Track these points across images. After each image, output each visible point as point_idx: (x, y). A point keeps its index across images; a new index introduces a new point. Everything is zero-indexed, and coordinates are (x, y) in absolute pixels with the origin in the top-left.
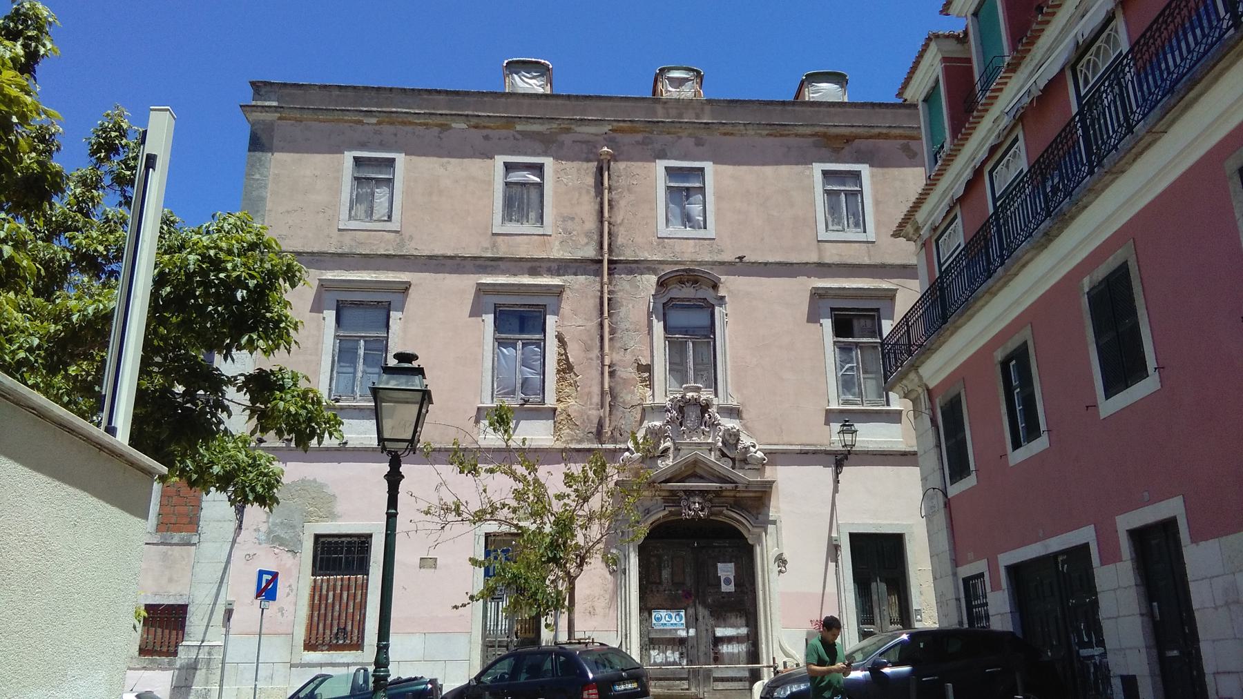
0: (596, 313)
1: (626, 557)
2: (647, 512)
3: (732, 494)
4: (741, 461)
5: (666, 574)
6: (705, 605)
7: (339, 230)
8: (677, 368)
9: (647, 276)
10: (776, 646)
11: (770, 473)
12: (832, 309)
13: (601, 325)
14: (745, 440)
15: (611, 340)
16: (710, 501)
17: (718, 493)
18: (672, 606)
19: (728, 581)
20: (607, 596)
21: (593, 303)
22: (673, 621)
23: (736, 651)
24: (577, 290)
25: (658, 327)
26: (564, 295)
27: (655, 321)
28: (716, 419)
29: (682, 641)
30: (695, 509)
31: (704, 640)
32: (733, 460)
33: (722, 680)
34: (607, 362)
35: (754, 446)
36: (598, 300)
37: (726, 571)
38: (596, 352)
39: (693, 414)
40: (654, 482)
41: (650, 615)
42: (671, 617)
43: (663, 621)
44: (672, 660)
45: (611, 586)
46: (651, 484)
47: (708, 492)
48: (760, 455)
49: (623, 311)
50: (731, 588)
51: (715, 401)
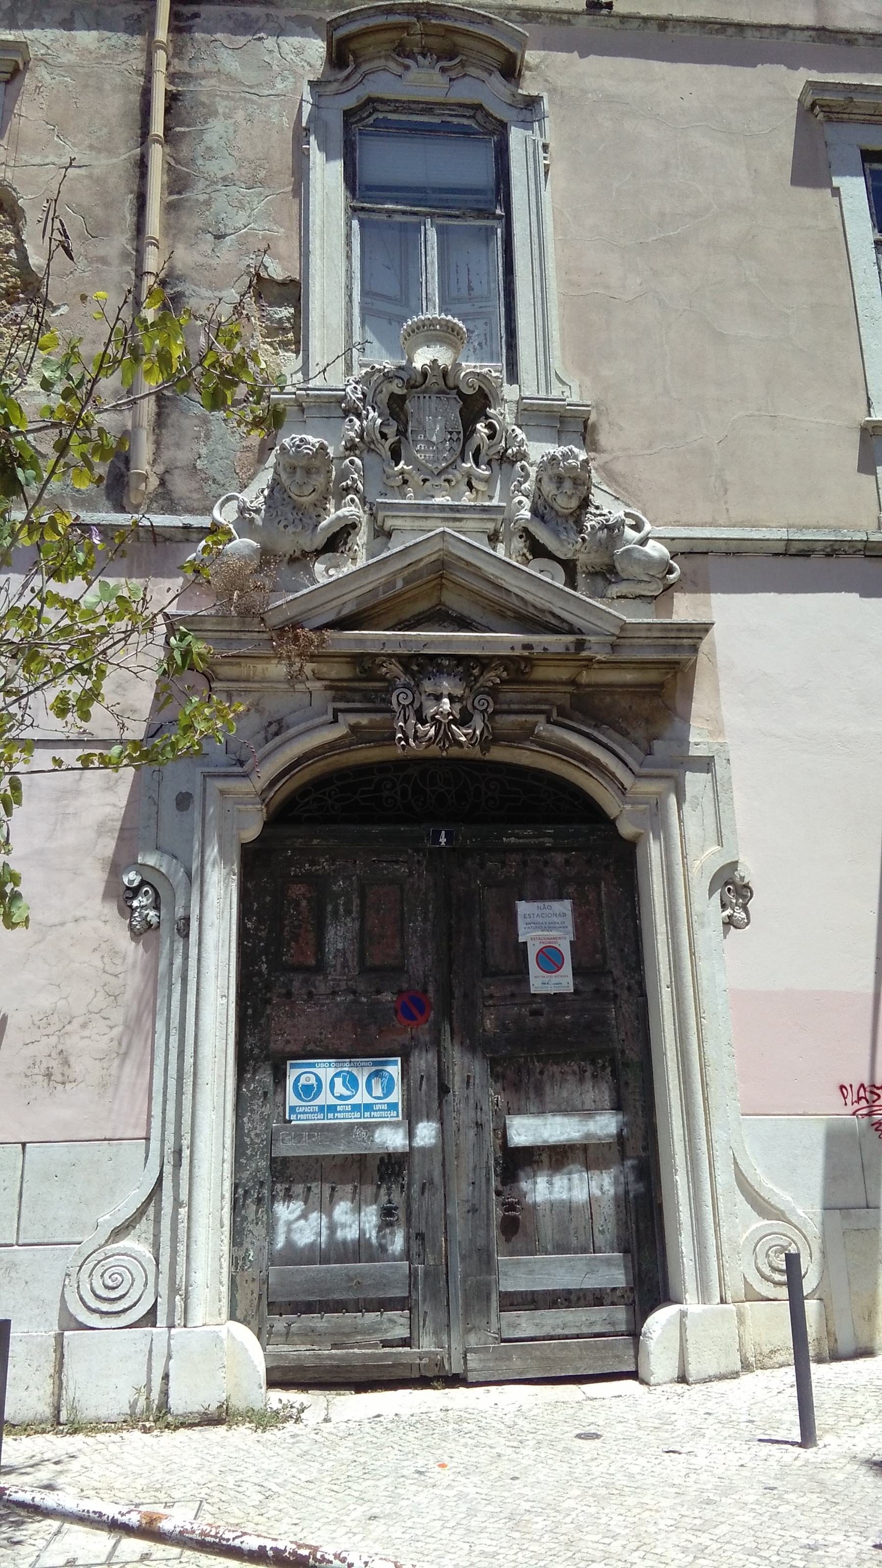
0: (126, 134)
1: (194, 878)
2: (276, 729)
3: (564, 674)
4: (593, 574)
5: (339, 937)
6: (474, 1042)
7: (808, 1438)
8: (383, 301)
9: (296, 40)
10: (725, 1178)
11: (684, 609)
12: (868, 156)
13: (142, 165)
14: (607, 506)
15: (170, 208)
16: (493, 692)
17: (517, 667)
18: (358, 1042)
19: (550, 959)
20: (117, 1016)
21: (117, 104)
22: (362, 1097)
23: (580, 1195)
24: (70, 69)
25: (327, 175)
26: (28, 80)
27: (317, 156)
28: (511, 439)
29: (392, 1166)
30: (436, 720)
31: (467, 1162)
32: (569, 567)
33: (532, 1301)
34: (153, 261)
35: (637, 527)
36: (135, 98)
37: (545, 926)
38: (122, 240)
39: (435, 423)
40: (296, 625)
41: (280, 1077)
42: (352, 1083)
43: (325, 1098)
44: (351, 1234)
45: (134, 981)
46: (288, 630)
47: (484, 663)
48: (655, 550)
49: (215, 132)
50: (563, 981)
51: (510, 392)
